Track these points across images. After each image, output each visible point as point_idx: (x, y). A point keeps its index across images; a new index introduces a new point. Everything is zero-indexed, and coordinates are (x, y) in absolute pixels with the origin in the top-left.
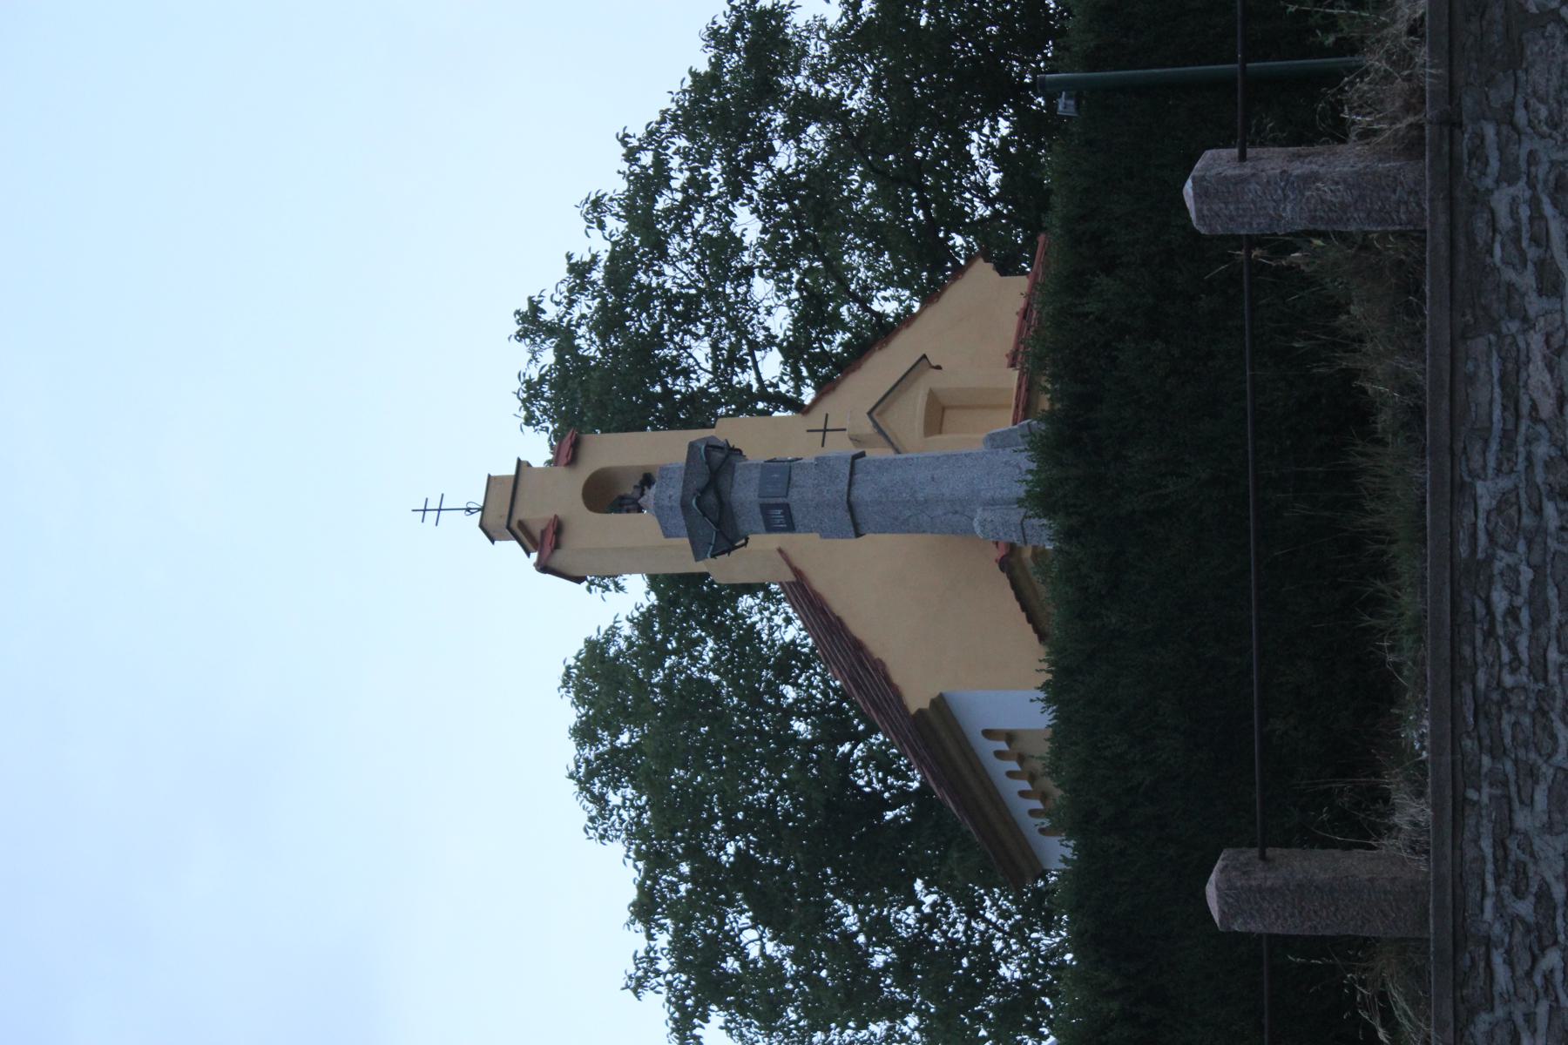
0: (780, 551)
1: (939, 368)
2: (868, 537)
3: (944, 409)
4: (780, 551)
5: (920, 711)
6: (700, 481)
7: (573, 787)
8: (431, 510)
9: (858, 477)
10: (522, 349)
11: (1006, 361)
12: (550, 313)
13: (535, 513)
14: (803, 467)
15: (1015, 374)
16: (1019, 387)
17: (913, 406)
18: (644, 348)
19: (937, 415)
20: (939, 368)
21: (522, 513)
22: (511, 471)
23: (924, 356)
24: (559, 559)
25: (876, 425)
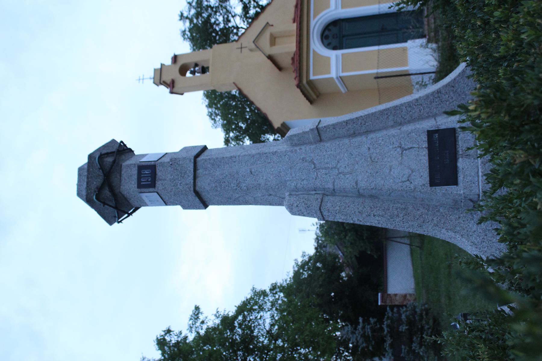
0: (234, 83)
1: (272, 25)
2: (210, 207)
3: (275, 38)
4: (234, 83)
5: (278, 128)
6: (98, 182)
7: (208, 118)
8: (141, 79)
9: (200, 172)
10: (181, 23)
11: (292, 21)
12: (185, 14)
13: (167, 78)
14: (162, 164)
15: (295, 24)
16: (297, 29)
17: (266, 37)
18: (207, 21)
19: (273, 41)
20: (272, 25)
21: (164, 78)
22: (159, 67)
23: (268, 23)
24: (175, 90)
25: (256, 45)
